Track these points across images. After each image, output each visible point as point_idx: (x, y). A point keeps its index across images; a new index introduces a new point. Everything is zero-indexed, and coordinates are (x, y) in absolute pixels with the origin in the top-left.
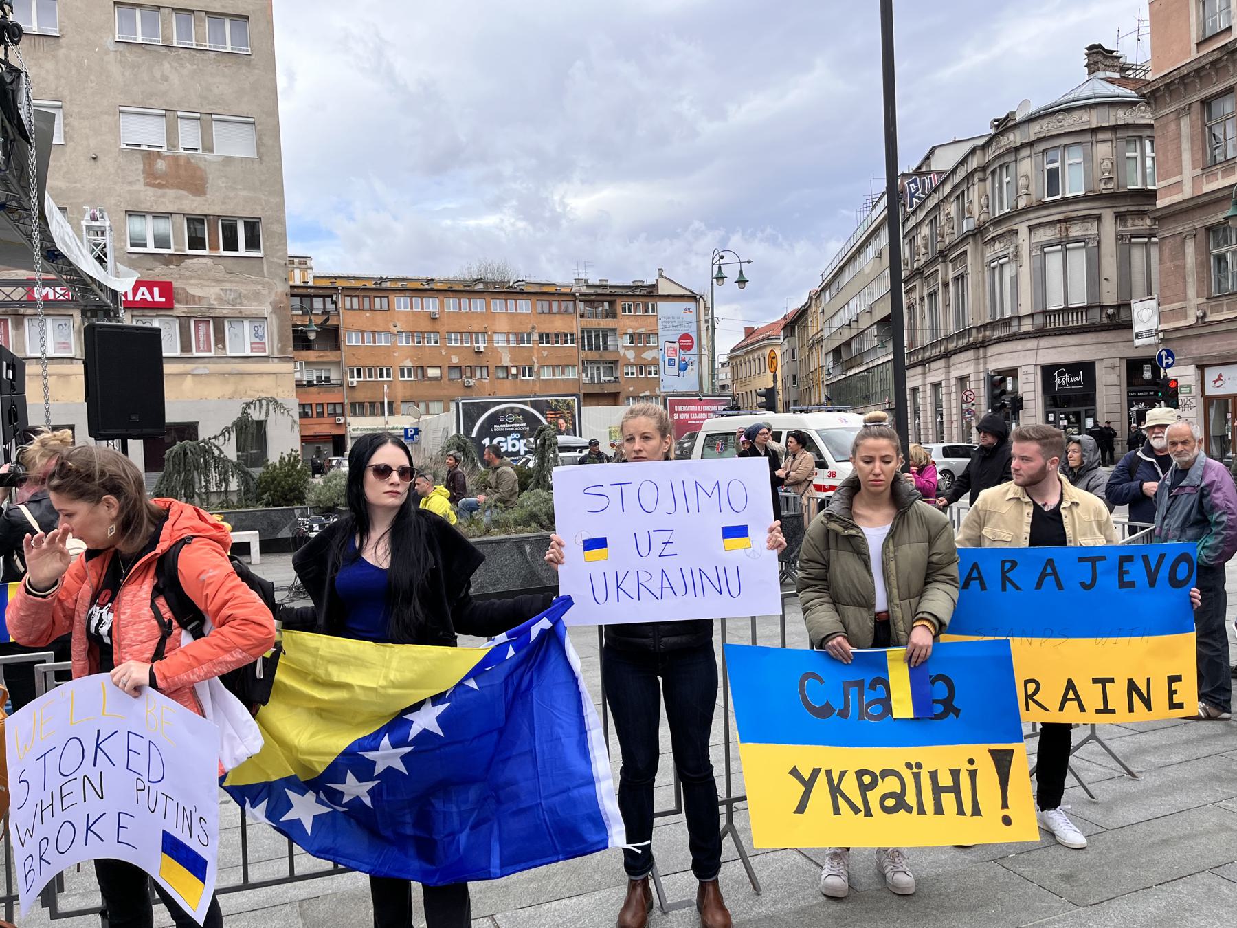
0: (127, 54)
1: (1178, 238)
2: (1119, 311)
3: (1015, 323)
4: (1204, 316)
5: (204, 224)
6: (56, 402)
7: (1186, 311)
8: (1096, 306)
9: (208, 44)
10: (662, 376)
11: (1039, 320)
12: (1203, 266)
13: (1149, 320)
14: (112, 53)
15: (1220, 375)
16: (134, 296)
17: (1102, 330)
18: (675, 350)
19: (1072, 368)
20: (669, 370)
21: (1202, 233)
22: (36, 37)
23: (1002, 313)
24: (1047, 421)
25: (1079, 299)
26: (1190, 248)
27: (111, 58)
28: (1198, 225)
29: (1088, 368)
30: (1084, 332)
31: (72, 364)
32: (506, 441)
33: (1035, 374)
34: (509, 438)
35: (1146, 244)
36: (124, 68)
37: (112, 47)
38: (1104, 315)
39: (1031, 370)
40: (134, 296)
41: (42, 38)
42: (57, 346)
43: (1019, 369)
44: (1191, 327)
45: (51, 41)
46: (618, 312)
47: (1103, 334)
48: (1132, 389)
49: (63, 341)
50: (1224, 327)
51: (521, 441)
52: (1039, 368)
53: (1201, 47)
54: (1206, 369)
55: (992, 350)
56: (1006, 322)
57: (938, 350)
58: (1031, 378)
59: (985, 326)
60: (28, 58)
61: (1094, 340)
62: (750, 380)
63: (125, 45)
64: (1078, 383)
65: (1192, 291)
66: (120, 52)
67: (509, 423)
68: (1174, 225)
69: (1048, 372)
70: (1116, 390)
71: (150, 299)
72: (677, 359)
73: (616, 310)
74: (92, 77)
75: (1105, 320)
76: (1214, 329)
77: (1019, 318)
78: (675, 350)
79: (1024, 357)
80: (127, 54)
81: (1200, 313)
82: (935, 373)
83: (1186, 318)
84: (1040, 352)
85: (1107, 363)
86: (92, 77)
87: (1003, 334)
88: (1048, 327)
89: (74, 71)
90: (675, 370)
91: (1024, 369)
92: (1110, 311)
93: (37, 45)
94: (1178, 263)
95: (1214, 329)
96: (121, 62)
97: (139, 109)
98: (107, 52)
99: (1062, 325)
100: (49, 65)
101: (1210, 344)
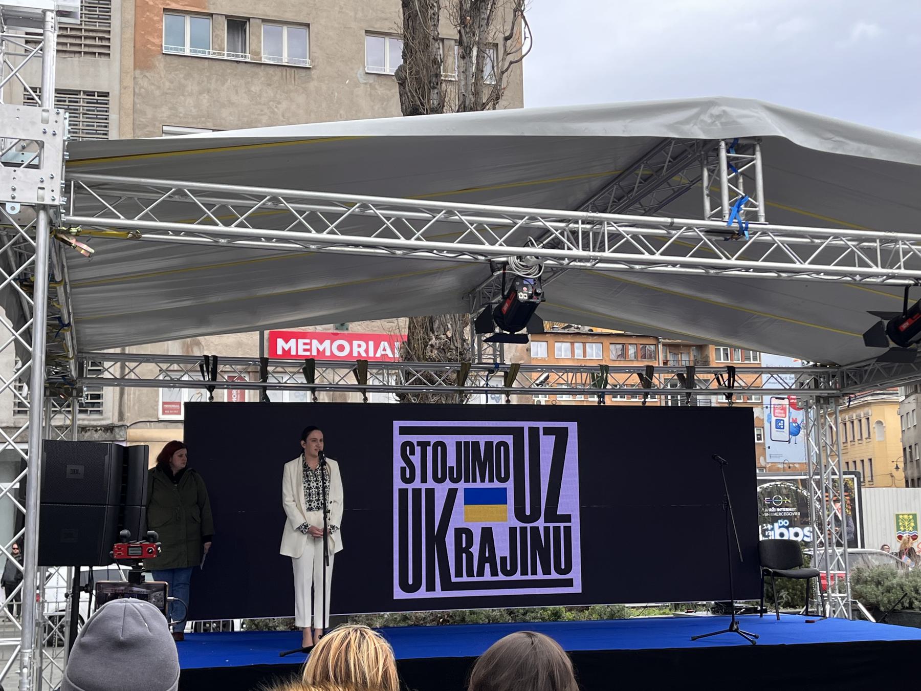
0: (377, 87)
5: (9, 241)
9: (226, 52)
10: (768, 442)
14: (362, 85)
16: (375, 352)
18: (784, 409)
20: (776, 434)
22: (288, 69)
27: (360, 91)
32: (772, 529)
34: (776, 525)
36: (373, 101)
37: (362, 79)
40: (375, 352)
41: (293, 70)
45: (303, 73)
46: (711, 359)
51: (790, 529)
60: (279, 91)
62: (846, 448)
63: (376, 77)
66: (371, 84)
67: (776, 507)
71: (391, 355)
72: (786, 420)
73: (707, 357)
74: (342, 112)
78: (784, 409)
80: (377, 87)
86: (342, 112)
89: (324, 105)
90: (785, 434)
93: (288, 77)
96: (370, 95)
98: (357, 84)
100: (301, 99)
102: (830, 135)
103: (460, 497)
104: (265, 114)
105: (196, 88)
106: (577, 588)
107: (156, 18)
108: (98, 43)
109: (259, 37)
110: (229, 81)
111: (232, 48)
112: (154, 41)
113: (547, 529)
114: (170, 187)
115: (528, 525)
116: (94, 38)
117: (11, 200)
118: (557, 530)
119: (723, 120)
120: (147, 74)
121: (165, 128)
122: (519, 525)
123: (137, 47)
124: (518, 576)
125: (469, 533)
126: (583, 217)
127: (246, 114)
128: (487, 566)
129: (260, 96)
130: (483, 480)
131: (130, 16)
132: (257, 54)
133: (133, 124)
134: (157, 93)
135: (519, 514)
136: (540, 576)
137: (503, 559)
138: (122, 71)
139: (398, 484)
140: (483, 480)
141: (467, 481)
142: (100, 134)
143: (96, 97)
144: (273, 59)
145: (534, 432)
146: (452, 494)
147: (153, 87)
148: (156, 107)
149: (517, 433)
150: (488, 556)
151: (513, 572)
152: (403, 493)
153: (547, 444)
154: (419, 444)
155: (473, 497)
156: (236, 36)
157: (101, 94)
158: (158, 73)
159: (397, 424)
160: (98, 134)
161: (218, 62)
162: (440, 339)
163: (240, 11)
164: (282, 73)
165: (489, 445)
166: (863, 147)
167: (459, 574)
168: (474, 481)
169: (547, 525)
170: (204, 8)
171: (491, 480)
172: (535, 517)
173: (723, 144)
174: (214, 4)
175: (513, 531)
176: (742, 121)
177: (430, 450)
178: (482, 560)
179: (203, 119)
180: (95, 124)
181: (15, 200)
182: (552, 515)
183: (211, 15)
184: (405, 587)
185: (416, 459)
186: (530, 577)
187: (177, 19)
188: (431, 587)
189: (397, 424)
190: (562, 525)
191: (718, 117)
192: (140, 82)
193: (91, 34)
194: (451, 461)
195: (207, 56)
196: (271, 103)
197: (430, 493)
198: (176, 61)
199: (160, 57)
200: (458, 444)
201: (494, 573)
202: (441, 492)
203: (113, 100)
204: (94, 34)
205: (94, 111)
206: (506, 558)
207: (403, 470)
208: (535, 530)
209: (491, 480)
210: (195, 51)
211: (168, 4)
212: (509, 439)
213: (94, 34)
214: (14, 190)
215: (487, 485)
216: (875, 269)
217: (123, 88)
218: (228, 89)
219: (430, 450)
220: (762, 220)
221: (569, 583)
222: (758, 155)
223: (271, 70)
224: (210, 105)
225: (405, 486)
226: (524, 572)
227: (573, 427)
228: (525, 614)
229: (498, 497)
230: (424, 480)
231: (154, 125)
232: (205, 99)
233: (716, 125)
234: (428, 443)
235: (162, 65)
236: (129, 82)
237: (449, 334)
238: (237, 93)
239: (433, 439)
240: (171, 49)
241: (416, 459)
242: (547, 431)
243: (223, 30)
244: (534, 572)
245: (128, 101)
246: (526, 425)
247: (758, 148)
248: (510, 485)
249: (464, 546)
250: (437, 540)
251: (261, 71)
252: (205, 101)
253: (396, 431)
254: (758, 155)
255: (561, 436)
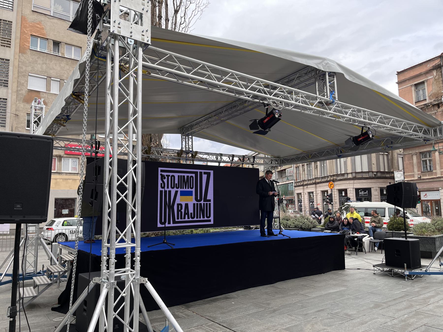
1: (410, 155)
2: (377, 173)
3: (346, 175)
4: (420, 177)
6: (71, 189)
7: (414, 176)
8: (371, 172)
9: (52, 52)
11: (354, 175)
12: (419, 163)
13: (400, 177)
15: (426, 194)
17: (373, 179)
19: (364, 190)
21: (418, 154)
23: (341, 171)
24: (420, 203)
25: (366, 169)
26: (415, 158)
28: (417, 151)
29: (369, 190)
30: (368, 179)
31: (78, 175)
33: (353, 191)
35: (383, 154)
38: (373, 174)
39: (352, 189)
41: (76, 61)
42: (72, 169)
43: (348, 189)
44: (416, 180)
47: (373, 180)
48: (382, 196)
49: (75, 167)
50: (427, 181)
52: (354, 189)
53: (416, 103)
54: (421, 192)
55: (336, 183)
56: (343, 175)
57: (312, 181)
58: (352, 192)
59: (334, 175)
61: (371, 182)
64: (366, 194)
65: (416, 170)
68: (408, 151)
69: (357, 190)
70: (377, 197)
75: (374, 176)
76: (424, 181)
77: (347, 174)
79: (349, 185)
81: (419, 176)
82: (309, 189)
83: (414, 177)
84: (355, 184)
85: (375, 188)
87: (341, 178)
88: (357, 177)
91: (349, 189)
92: (375, 173)
94: (410, 162)
95: (424, 181)
97: (38, 75)
99: (361, 177)
101: (423, 185)
102: (352, 76)
103: (179, 193)
104: (66, 74)
105: (41, 62)
106: (212, 222)
107: (28, 37)
108: (6, 42)
109: (64, 49)
110: (53, 61)
111: (54, 51)
112: (26, 44)
113: (204, 204)
114: (167, 54)
115: (199, 203)
116: (5, 41)
117: (130, 37)
118: (207, 204)
119: (328, 65)
120: (24, 55)
121: (29, 74)
122: (196, 202)
123: (20, 45)
124: (195, 219)
125: (181, 205)
126: (295, 90)
127: (59, 73)
128: (186, 216)
129: (64, 68)
130: (186, 188)
131: (19, 35)
132: (63, 54)
133: (18, 71)
134: (27, 62)
135: (196, 199)
136: (202, 219)
137: (191, 213)
138: (15, 53)
139: (160, 189)
140: (186, 188)
141: (181, 188)
142: (5, 73)
143: (5, 61)
144: (69, 56)
145: (201, 173)
146: (176, 192)
147: (26, 60)
148: (26, 66)
149: (196, 173)
150: (187, 213)
151: (194, 218)
152: (161, 192)
153: (205, 177)
154: (167, 175)
155: (183, 194)
156: (56, 47)
157: (6, 60)
158: (28, 55)
159: (160, 169)
160: (5, 73)
161: (49, 55)
162: (155, 144)
163: (58, 39)
164: (72, 62)
165: (188, 177)
166: (360, 81)
167: (178, 218)
168: (183, 188)
169: (204, 203)
170: (45, 36)
171: (188, 188)
172: (200, 200)
173: (327, 73)
174: (49, 35)
175: (194, 204)
176: (332, 66)
177: (170, 178)
178: (185, 214)
179: (44, 73)
180: (4, 70)
181: (132, 38)
182: (206, 200)
183: (48, 39)
184: (161, 223)
185: (165, 181)
186: (199, 219)
187: (35, 39)
188: (169, 223)
189: (160, 169)
190: (208, 203)
191: (327, 64)
192: (21, 57)
193: (4, 39)
194: (176, 182)
195: (46, 52)
196: (68, 71)
197: (170, 192)
198: (35, 52)
199: (29, 50)
200: (179, 176)
201: (188, 218)
202: (173, 191)
203: (11, 63)
204: (5, 39)
205: (3, 65)
206: (192, 213)
207: (161, 184)
208: (201, 204)
209: (188, 188)
210: (41, 50)
211: (32, 33)
212: (194, 175)
213: (5, 39)
214: (131, 33)
215: (187, 190)
216: (361, 119)
217: (15, 58)
218: (53, 64)
219: (170, 178)
220: (337, 100)
221: (210, 221)
222: (335, 79)
223: (68, 60)
224: (46, 68)
225: (162, 189)
226: (197, 218)
227: (212, 172)
228: (183, 231)
229: (190, 194)
230: (168, 188)
231: (26, 72)
232: (44, 66)
233: (326, 67)
234: (169, 176)
235: (29, 53)
236: (17, 57)
237: (158, 143)
238: (56, 65)
239: (171, 174)
240: (33, 48)
241: (165, 181)
242: (205, 173)
243: (52, 44)
244: (200, 218)
245: (17, 64)
246: (199, 171)
247: (335, 76)
248: (193, 190)
249: (180, 209)
250: (171, 207)
251: (64, 60)
252: (44, 67)
253: (159, 171)
254: (335, 79)
255: (209, 174)
